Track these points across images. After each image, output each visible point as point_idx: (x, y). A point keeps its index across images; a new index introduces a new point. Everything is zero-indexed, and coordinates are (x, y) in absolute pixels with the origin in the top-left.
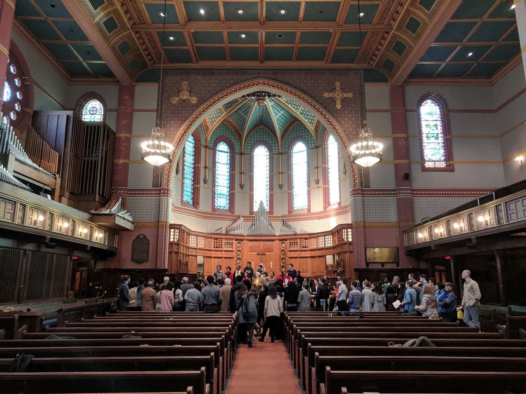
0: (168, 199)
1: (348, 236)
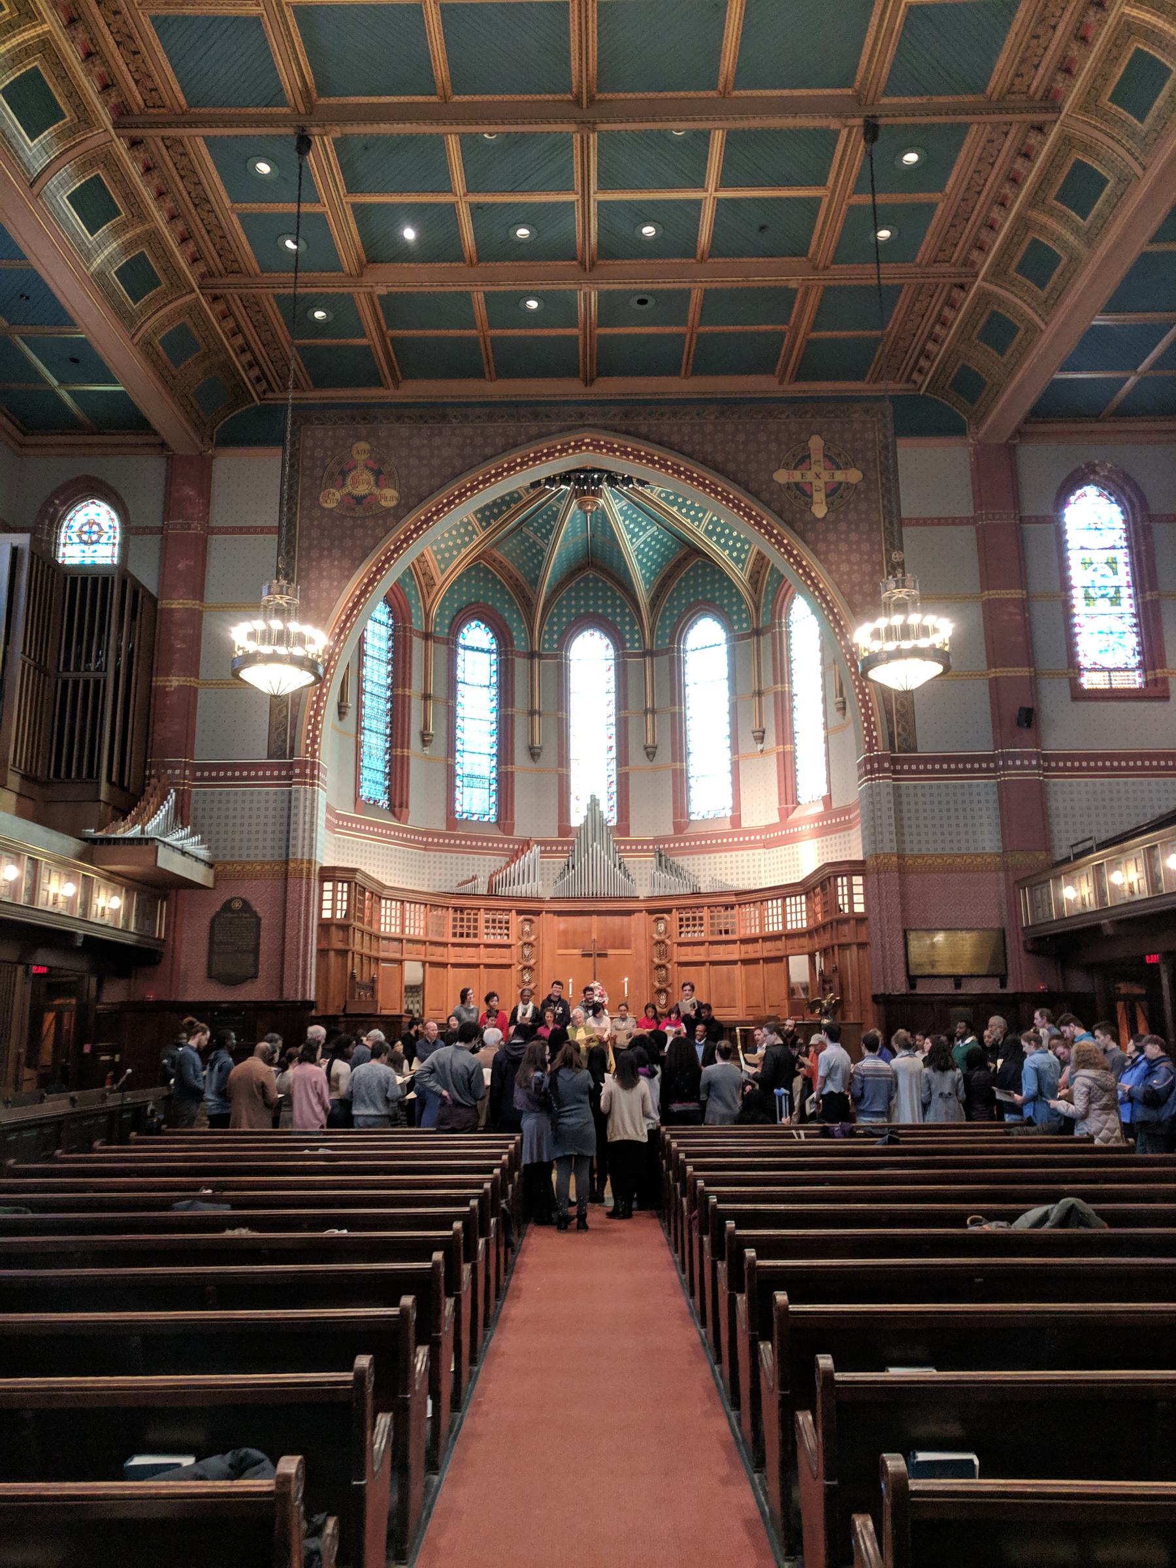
0: (314, 792)
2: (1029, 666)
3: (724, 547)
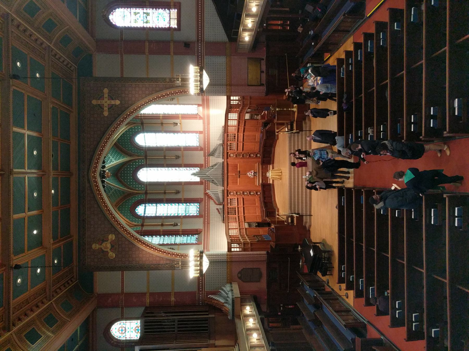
1: (235, 99)
2: (145, 42)
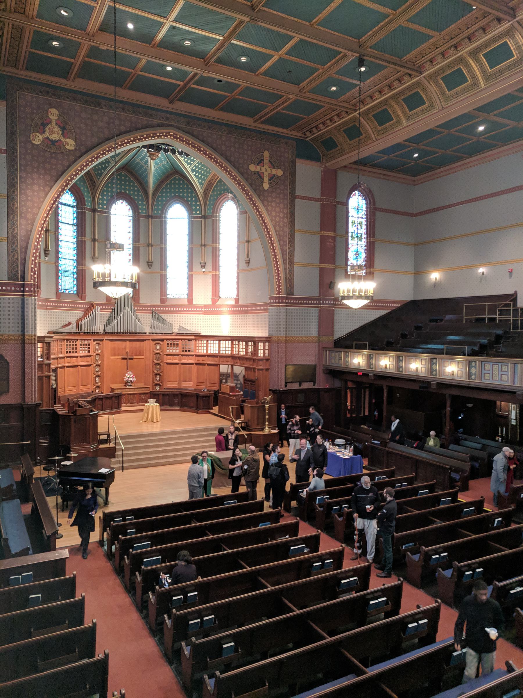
3: (197, 177)
